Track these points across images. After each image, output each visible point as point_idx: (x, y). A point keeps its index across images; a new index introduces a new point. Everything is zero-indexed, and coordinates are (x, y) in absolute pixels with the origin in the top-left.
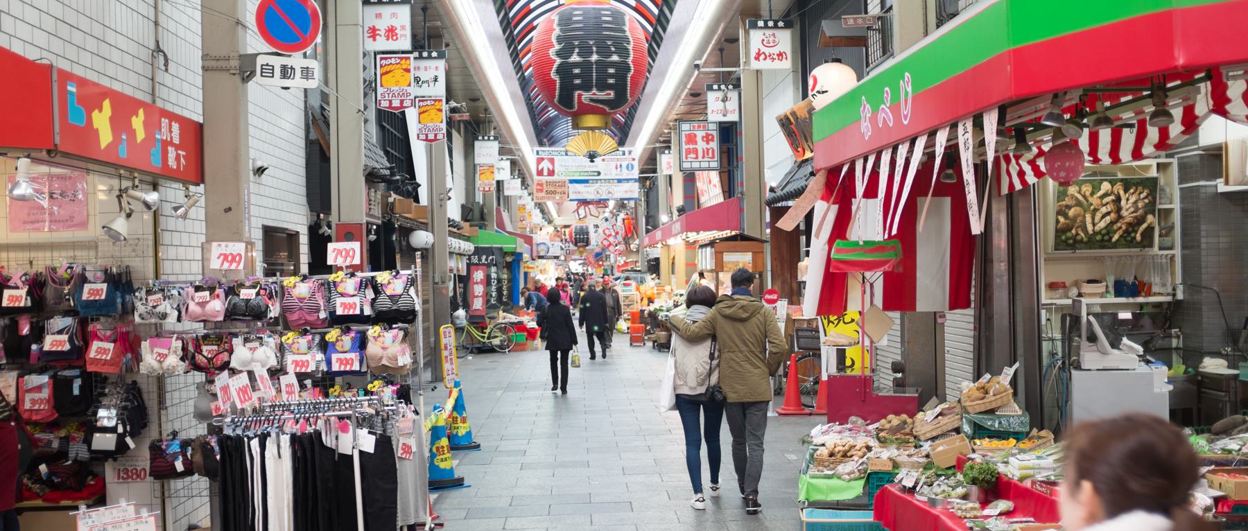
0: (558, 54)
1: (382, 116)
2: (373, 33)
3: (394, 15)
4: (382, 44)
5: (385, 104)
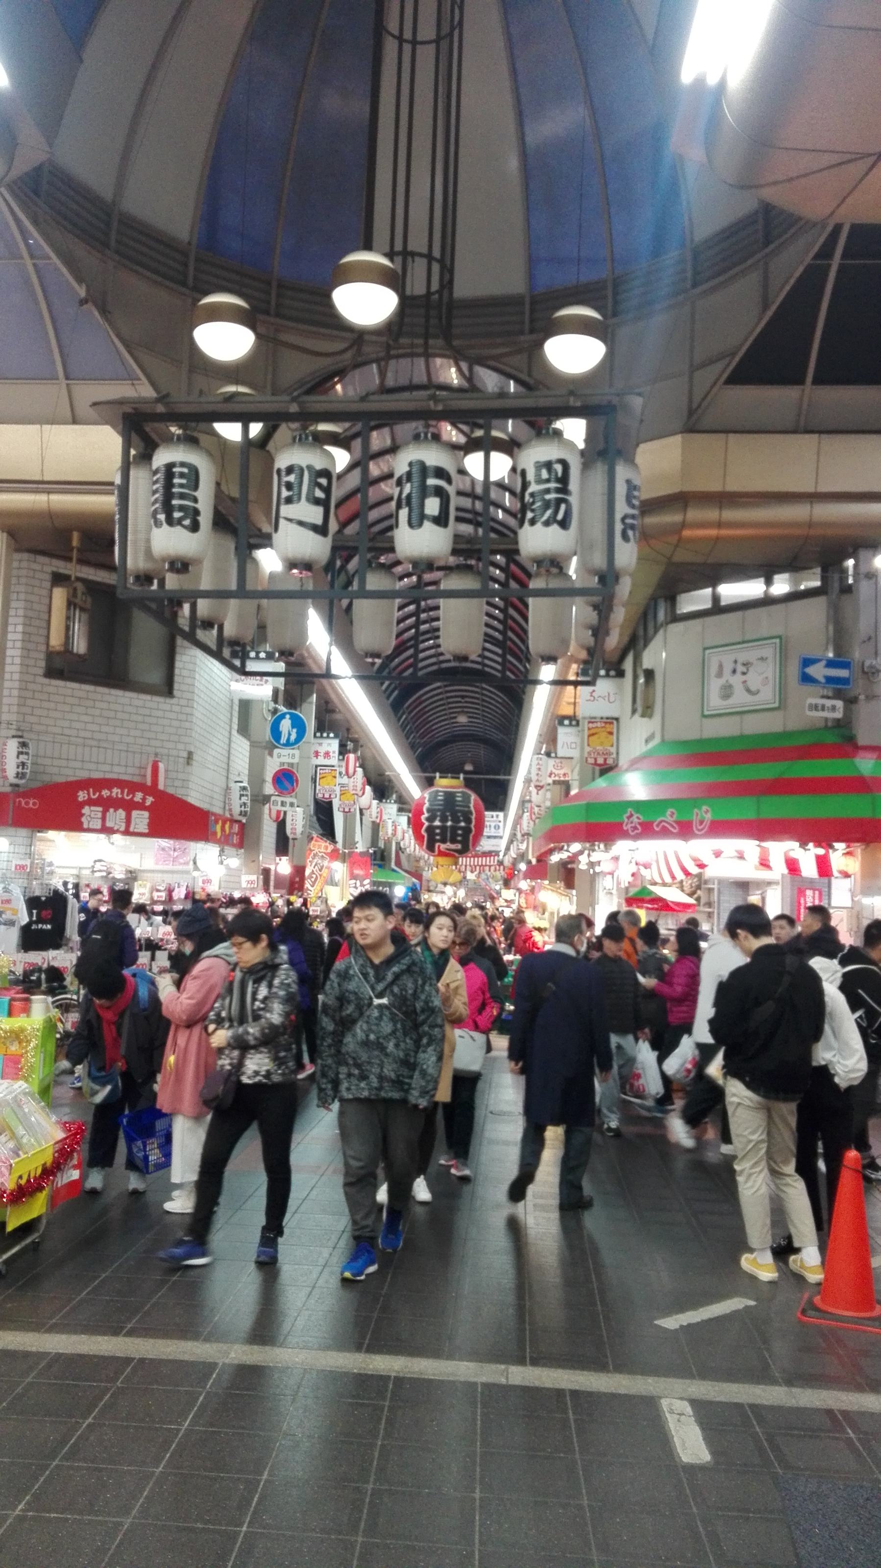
0: (428, 819)
1: (317, 803)
2: (317, 754)
3: (329, 744)
4: (321, 761)
5: (320, 796)
